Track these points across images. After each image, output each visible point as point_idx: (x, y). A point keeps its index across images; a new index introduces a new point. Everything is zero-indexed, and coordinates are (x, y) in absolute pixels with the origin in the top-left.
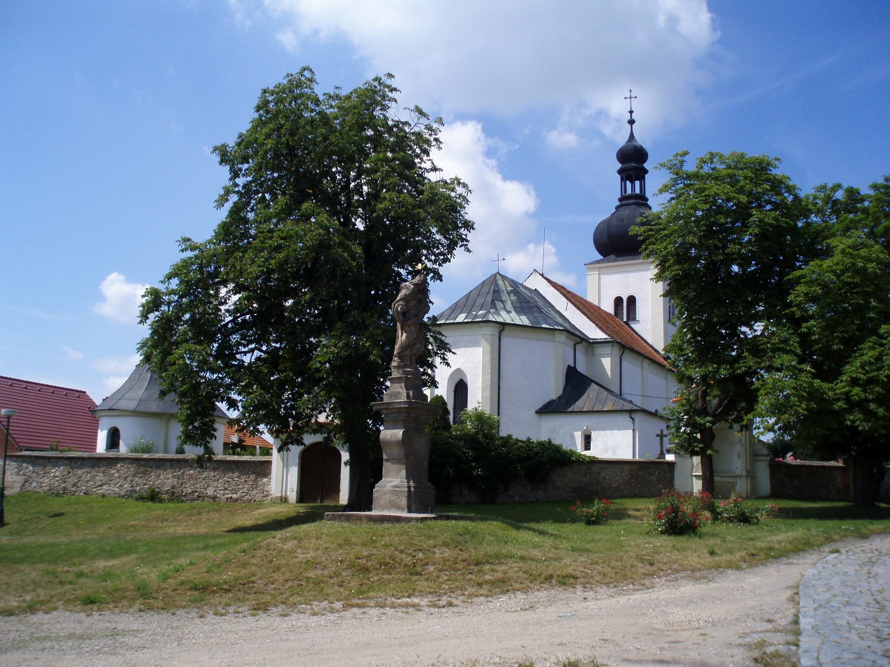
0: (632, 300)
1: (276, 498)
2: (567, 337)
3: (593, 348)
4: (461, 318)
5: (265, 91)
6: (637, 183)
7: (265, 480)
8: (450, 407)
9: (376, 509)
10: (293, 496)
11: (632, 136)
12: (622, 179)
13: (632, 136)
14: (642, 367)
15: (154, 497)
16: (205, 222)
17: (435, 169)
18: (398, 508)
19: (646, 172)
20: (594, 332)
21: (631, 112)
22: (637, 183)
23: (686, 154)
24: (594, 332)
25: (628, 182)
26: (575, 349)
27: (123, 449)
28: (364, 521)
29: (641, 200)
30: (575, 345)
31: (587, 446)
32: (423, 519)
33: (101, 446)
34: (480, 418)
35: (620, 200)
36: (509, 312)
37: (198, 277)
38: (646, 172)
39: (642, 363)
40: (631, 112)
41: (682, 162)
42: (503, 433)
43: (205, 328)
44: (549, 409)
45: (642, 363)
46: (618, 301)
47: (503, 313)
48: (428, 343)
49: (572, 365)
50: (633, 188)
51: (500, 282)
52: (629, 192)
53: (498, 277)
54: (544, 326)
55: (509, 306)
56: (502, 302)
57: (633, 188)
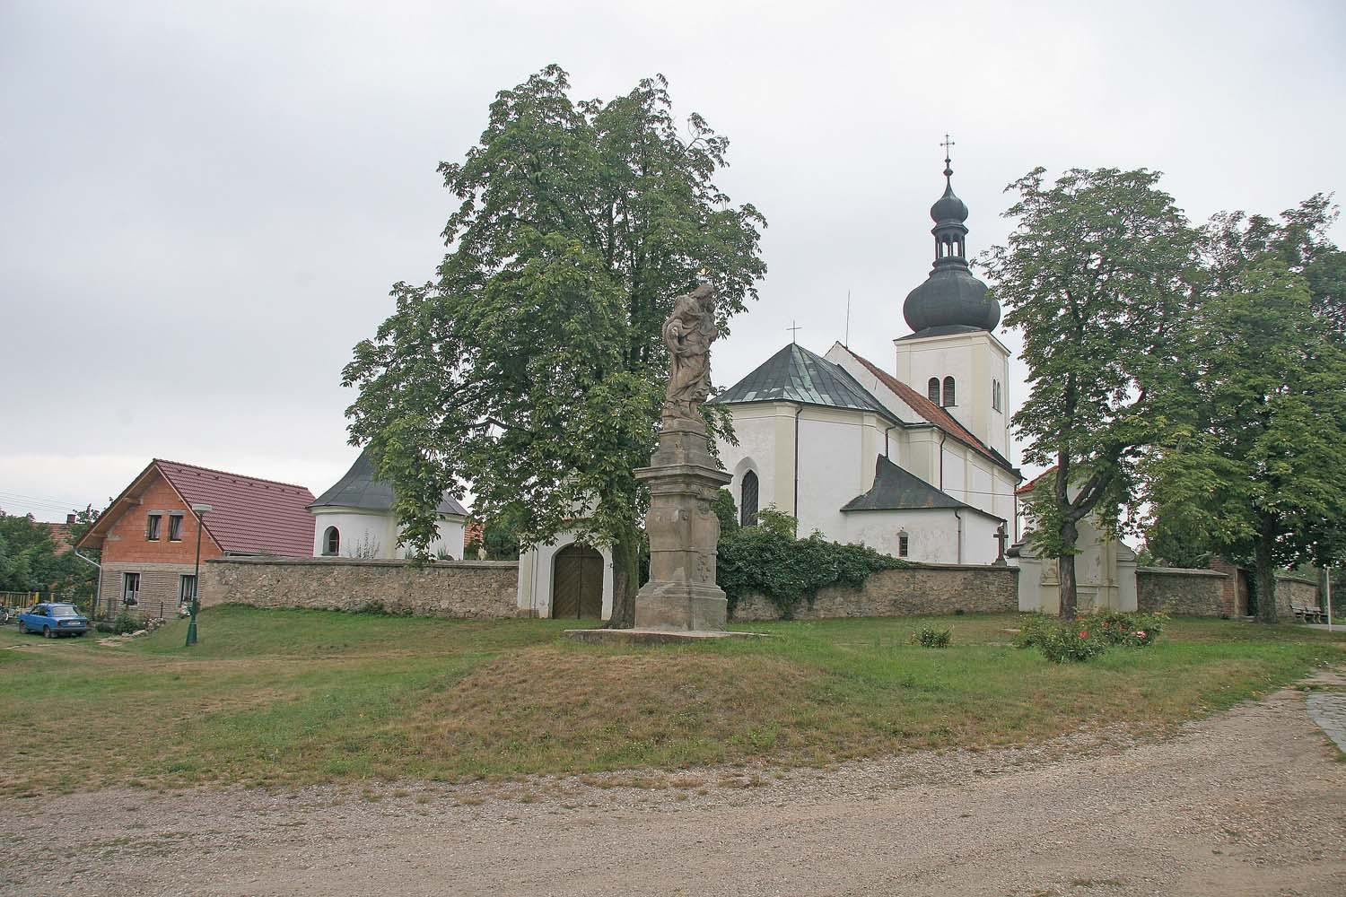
0: (949, 381)
1: (525, 612)
2: (878, 420)
3: (908, 434)
4: (750, 396)
5: (503, 94)
6: (955, 245)
7: (511, 590)
8: (738, 503)
9: (639, 625)
10: (544, 612)
11: (949, 189)
12: (937, 240)
13: (949, 189)
14: (966, 460)
15: (376, 610)
16: (422, 259)
17: (719, 198)
18: (672, 624)
19: (966, 231)
20: (908, 415)
21: (948, 161)
22: (955, 245)
23: (1040, 170)
24: (908, 415)
25: (944, 244)
26: (887, 435)
27: (343, 552)
28: (622, 643)
29: (960, 263)
30: (887, 430)
31: (904, 552)
32: (911, 344)
33: (318, 551)
34: (773, 517)
35: (934, 264)
36: (807, 390)
37: (418, 324)
38: (966, 231)
39: (965, 452)
40: (948, 161)
41: (1037, 181)
42: (803, 533)
43: (430, 393)
44: (852, 508)
45: (965, 452)
46: (933, 383)
47: (801, 391)
48: (714, 411)
49: (884, 455)
50: (950, 250)
51: (797, 355)
52: (945, 254)
53: (794, 349)
54: (849, 406)
55: (808, 383)
56: (800, 377)
57: (950, 250)
